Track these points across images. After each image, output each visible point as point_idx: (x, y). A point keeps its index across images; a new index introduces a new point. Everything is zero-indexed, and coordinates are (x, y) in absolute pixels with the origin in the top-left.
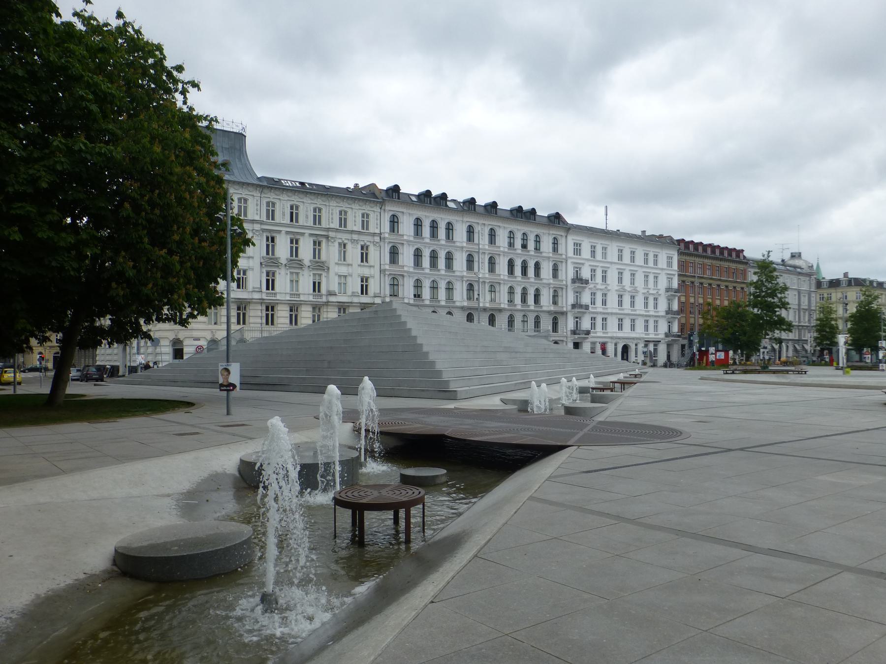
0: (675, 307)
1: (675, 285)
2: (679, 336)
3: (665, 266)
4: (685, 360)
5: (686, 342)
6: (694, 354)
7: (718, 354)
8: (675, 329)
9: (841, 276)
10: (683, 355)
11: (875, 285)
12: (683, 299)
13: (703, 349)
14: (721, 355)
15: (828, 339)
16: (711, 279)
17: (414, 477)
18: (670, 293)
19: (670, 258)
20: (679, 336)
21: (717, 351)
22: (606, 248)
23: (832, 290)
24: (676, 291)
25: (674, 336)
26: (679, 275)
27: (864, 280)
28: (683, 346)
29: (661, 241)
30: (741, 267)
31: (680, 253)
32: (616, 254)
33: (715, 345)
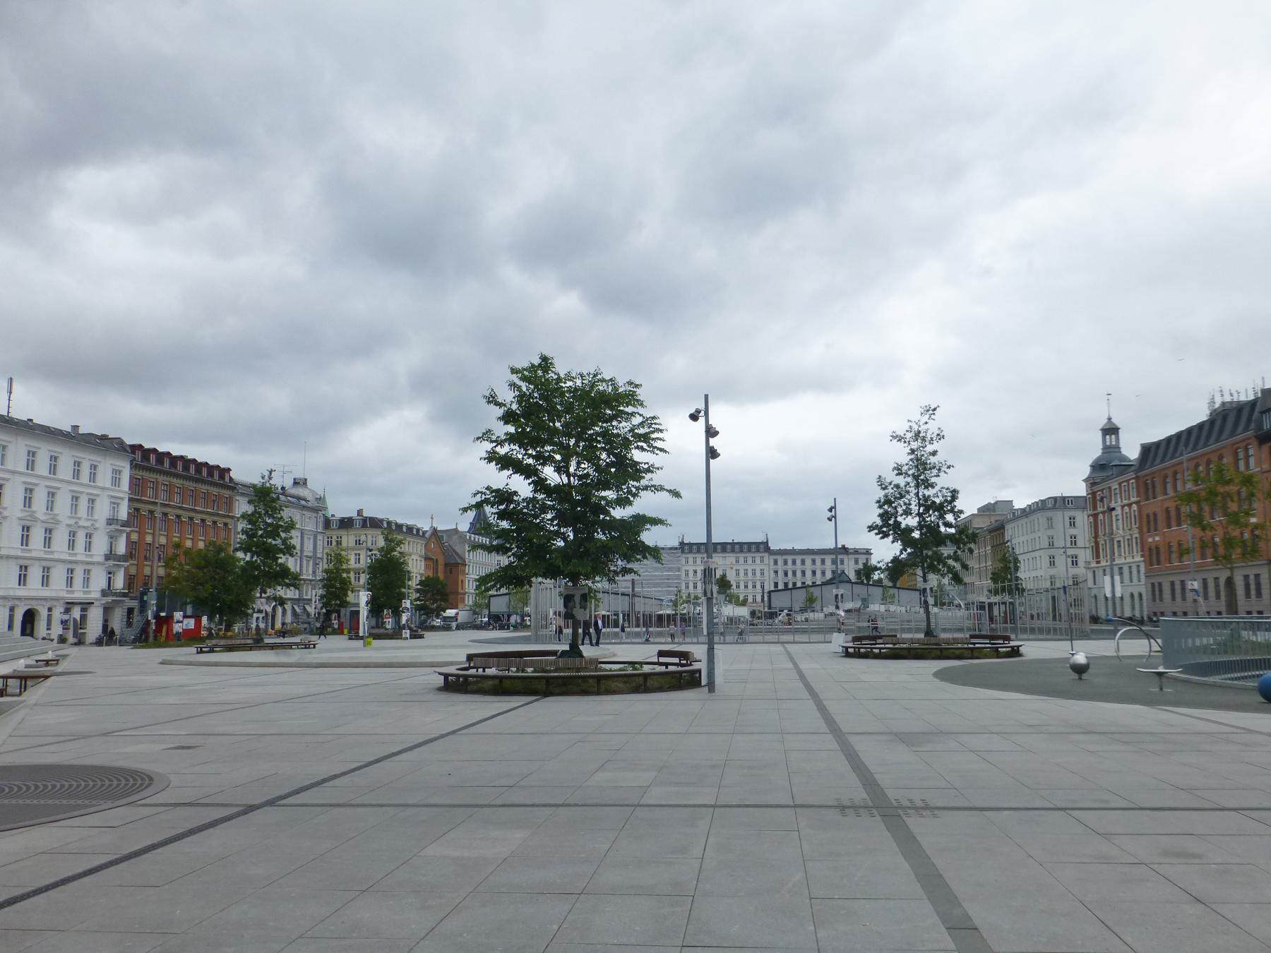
2: (124, 595)
3: (108, 484)
4: (131, 634)
6: (148, 623)
9: (354, 515)
10: (129, 624)
12: (134, 537)
14: (190, 624)
18: (113, 527)
20: (124, 595)
23: (343, 532)
24: (125, 524)
25: (115, 594)
26: (130, 500)
27: (381, 521)
28: (130, 611)
29: (104, 444)
30: (226, 493)
31: (134, 466)
32: (109, 475)
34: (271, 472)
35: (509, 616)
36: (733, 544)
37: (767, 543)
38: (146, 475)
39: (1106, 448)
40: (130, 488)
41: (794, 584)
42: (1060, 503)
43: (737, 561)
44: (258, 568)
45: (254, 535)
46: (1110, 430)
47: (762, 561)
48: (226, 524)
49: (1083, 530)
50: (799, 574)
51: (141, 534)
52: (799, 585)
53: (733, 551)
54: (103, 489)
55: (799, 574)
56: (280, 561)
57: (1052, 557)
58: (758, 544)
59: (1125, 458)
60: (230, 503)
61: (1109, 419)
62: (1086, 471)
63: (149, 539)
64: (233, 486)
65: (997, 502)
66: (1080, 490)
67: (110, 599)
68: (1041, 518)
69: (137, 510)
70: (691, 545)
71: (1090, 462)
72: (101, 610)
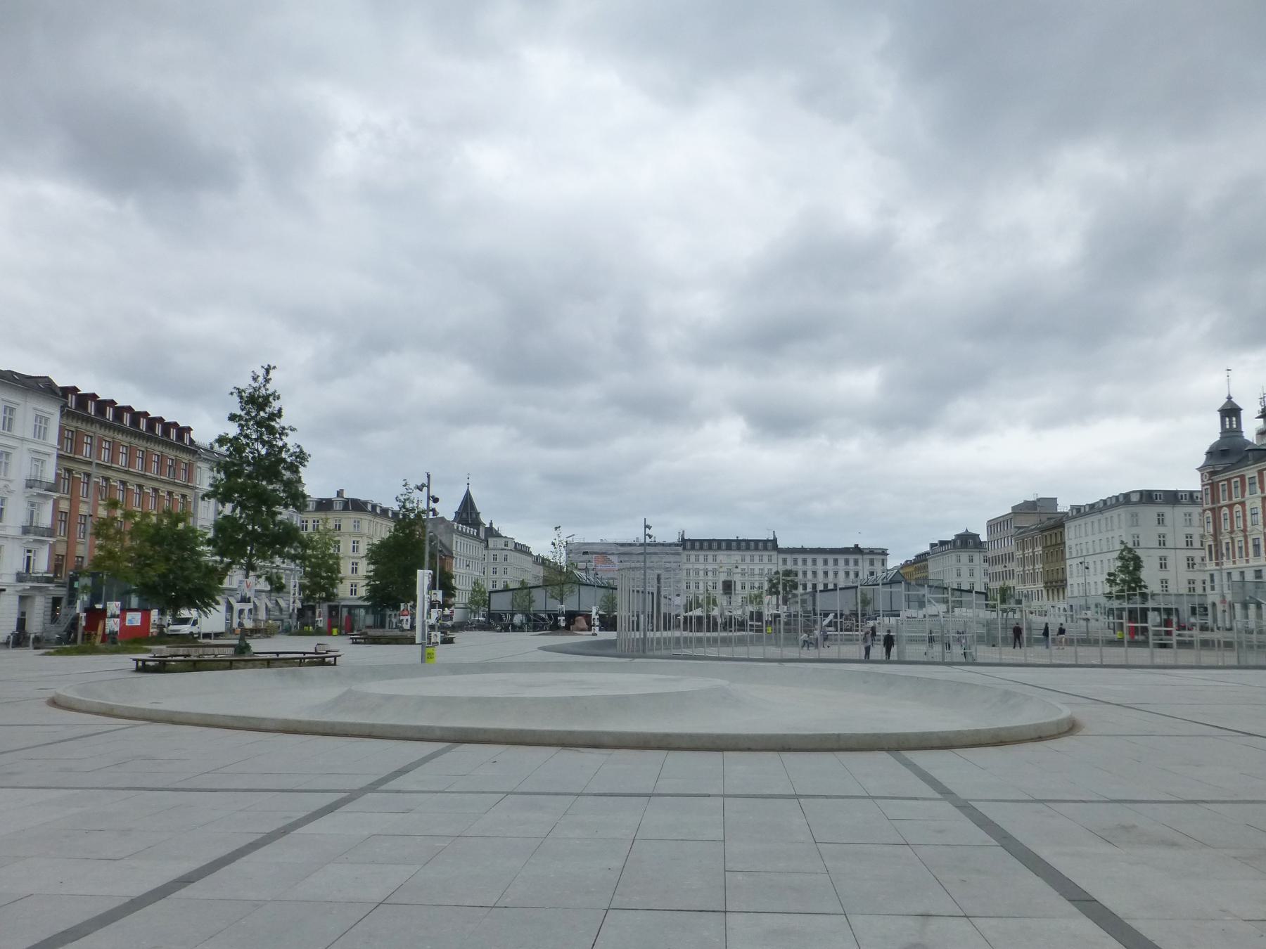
0: (46, 520)
1: (49, 474)
2: (48, 580)
3: (29, 434)
4: (55, 632)
5: (62, 592)
6: (76, 618)
7: (129, 616)
8: (42, 564)
9: (333, 495)
10: (54, 619)
11: (378, 510)
12: (64, 506)
13: (99, 606)
14: (134, 619)
15: (323, 589)
16: (156, 480)
17: (414, 584)
18: (35, 491)
19: (41, 420)
20: (48, 580)
21: (125, 609)
22: (12, 410)
23: (321, 515)
24: (52, 488)
25: (37, 579)
26: (60, 457)
27: (365, 503)
28: (56, 601)
29: (41, 387)
30: (185, 457)
31: (66, 413)
32: (31, 422)
33: (123, 596)
34: (268, 371)
35: (513, 615)
36: (738, 542)
37: (775, 540)
38: (82, 426)
39: (1224, 431)
40: (60, 441)
41: (826, 585)
42: (1173, 498)
43: (743, 560)
44: (242, 527)
45: (239, 474)
46: (1230, 412)
47: (770, 560)
48: (184, 496)
49: (1200, 528)
50: (831, 574)
51: (74, 502)
52: (831, 586)
53: (739, 548)
54: (22, 440)
55: (809, 575)
56: (279, 517)
57: (959, 570)
58: (766, 542)
59: (1248, 443)
60: (189, 470)
61: (1229, 398)
62: (1201, 459)
63: (84, 509)
64: (193, 449)
65: (1039, 500)
66: (1193, 483)
67: (28, 585)
68: (1123, 512)
69: (69, 471)
70: (693, 542)
71: (1207, 448)
72: (15, 600)
